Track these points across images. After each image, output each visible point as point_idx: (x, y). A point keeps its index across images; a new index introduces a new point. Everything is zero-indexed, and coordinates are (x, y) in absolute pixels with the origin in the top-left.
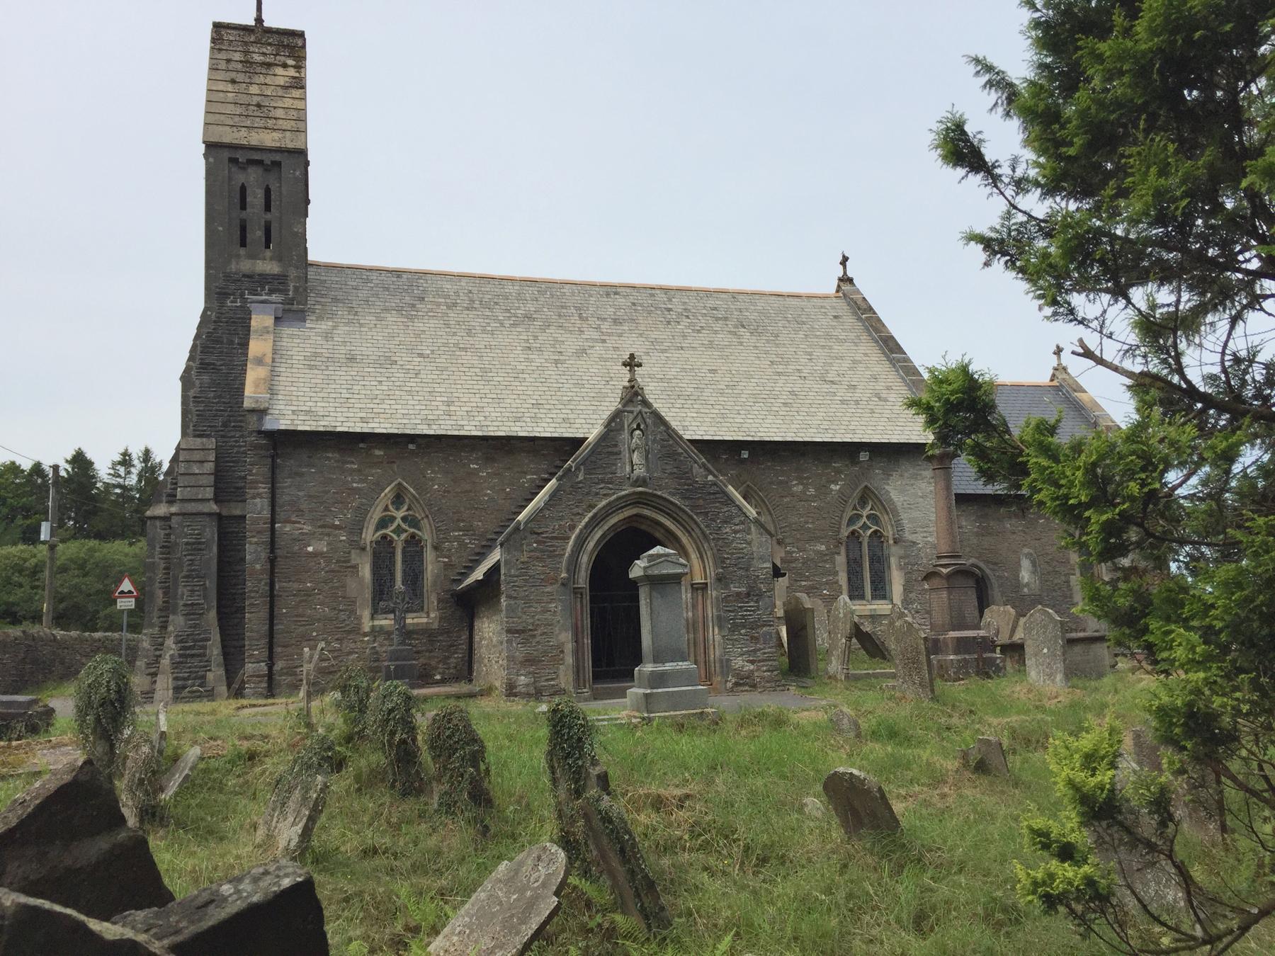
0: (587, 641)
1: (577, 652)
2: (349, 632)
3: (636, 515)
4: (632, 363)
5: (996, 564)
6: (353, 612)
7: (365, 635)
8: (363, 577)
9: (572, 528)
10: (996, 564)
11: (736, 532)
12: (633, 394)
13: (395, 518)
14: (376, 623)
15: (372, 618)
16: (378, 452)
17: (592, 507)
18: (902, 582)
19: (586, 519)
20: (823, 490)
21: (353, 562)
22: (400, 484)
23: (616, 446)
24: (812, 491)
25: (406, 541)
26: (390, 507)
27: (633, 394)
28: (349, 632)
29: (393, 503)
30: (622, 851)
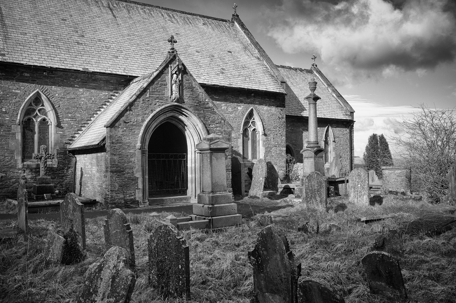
0: (147, 177)
1: (143, 182)
2: (11, 168)
3: (171, 116)
4: (172, 41)
5: (295, 145)
6: (12, 157)
7: (19, 169)
8: (18, 140)
9: (143, 121)
10: (295, 145)
11: (217, 127)
12: (173, 57)
13: (35, 110)
14: (25, 163)
15: (23, 161)
16: (26, 75)
17: (152, 111)
18: (264, 151)
19: (150, 117)
20: (235, 109)
21: (13, 131)
22: (38, 92)
23: (165, 81)
24: (230, 110)
25: (40, 122)
26: (33, 104)
27: (173, 57)
28: (11, 168)
29: (34, 102)
30: (41, 262)
